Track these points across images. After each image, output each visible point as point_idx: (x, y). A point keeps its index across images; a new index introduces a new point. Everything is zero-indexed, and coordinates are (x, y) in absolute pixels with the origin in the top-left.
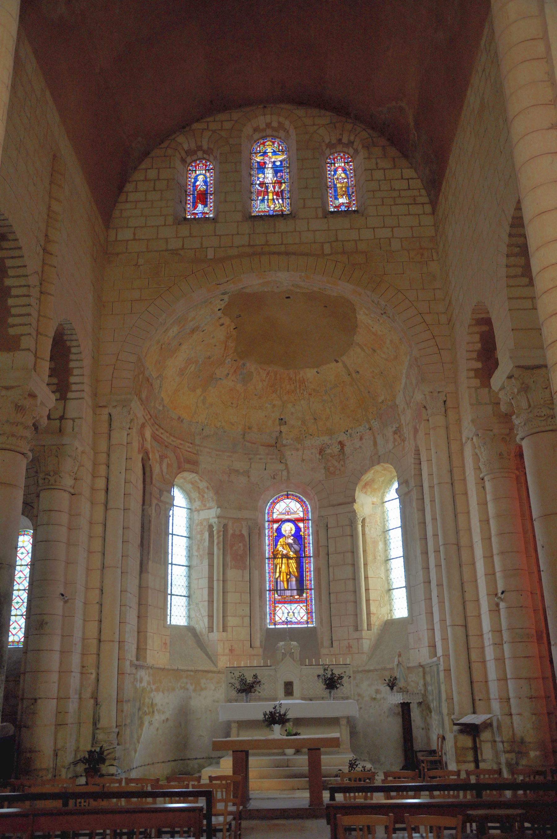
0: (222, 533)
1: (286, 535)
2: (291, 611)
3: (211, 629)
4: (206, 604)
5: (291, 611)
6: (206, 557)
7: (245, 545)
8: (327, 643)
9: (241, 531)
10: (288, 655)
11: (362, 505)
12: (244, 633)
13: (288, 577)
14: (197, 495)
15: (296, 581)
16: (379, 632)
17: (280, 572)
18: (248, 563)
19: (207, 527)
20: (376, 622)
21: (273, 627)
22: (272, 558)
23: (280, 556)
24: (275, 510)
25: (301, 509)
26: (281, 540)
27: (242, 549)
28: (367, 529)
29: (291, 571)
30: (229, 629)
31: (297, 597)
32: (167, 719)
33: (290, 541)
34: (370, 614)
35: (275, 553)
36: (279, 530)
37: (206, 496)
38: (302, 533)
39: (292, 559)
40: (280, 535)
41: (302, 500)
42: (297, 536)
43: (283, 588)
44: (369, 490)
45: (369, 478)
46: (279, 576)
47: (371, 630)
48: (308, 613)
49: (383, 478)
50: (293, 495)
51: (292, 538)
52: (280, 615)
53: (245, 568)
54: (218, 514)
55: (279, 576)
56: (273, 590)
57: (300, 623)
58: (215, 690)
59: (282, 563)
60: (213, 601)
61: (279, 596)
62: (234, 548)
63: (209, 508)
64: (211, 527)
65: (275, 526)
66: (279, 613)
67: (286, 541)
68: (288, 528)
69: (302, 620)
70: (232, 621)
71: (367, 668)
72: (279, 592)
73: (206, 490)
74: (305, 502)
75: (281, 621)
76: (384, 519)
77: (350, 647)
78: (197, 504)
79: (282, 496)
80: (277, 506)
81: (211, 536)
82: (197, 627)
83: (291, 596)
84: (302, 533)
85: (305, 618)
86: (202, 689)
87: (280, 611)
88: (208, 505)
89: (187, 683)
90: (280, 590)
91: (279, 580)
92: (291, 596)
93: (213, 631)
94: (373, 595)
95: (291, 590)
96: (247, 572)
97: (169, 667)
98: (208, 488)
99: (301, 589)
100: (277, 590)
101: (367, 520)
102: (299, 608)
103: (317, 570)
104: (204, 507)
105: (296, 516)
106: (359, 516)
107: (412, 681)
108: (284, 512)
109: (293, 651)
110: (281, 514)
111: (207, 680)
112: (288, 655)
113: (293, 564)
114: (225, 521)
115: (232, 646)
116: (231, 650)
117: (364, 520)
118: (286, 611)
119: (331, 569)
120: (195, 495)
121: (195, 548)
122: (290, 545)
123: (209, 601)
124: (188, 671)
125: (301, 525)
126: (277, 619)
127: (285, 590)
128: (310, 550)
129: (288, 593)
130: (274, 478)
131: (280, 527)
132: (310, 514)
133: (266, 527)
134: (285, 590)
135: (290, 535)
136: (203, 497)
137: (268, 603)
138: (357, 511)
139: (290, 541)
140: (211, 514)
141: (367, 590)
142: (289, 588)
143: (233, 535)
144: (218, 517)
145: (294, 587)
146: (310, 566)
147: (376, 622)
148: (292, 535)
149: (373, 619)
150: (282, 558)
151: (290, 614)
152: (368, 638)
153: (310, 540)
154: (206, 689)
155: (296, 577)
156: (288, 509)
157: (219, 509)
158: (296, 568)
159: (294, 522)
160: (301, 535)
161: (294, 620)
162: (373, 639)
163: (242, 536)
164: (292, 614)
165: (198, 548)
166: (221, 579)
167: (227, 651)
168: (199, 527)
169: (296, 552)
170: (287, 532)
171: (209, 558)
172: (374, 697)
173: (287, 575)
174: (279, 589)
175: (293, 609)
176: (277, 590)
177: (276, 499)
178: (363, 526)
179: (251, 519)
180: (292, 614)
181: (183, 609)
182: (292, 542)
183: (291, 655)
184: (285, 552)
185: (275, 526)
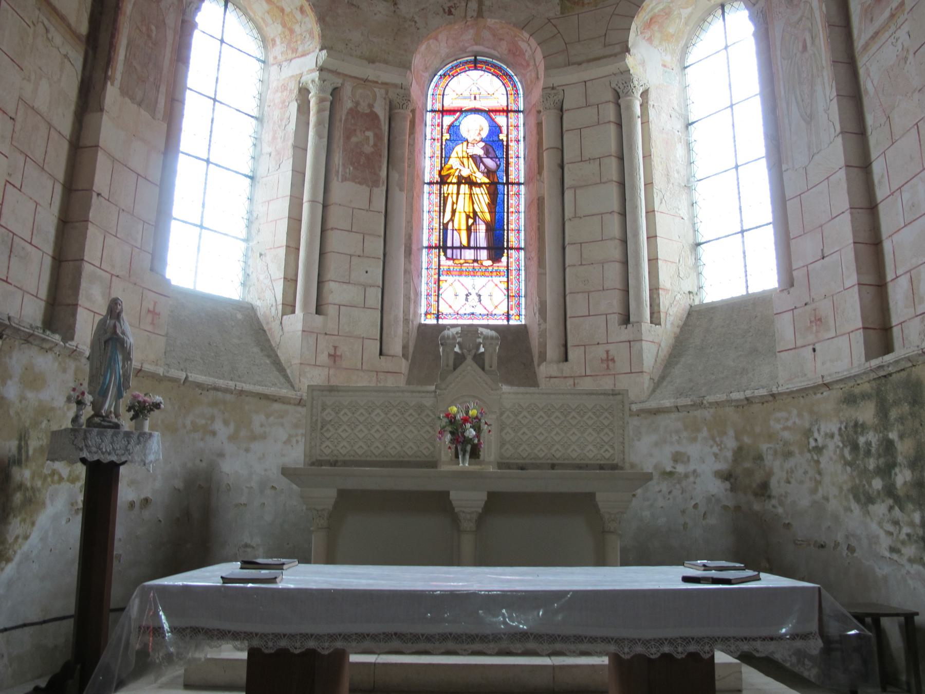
0: (328, 104)
1: (470, 140)
2: (473, 292)
3: (289, 307)
4: (282, 252)
6: (289, 152)
7: (378, 137)
8: (552, 352)
9: (371, 106)
10: (469, 360)
11: (643, 63)
12: (368, 322)
14: (280, 28)
15: (487, 230)
16: (678, 330)
17: (454, 212)
18: (384, 173)
19: (296, 91)
20: (673, 306)
21: (434, 322)
22: (437, 183)
27: (372, 142)
28: (652, 113)
29: (477, 209)
30: (331, 310)
32: (146, 501)
33: (478, 150)
34: (658, 289)
35: (444, 173)
37: (297, 28)
38: (503, 137)
39: (479, 185)
41: (507, 74)
42: (494, 144)
43: (458, 245)
44: (658, 35)
45: (661, 7)
46: (452, 220)
47: (660, 324)
49: (689, 10)
50: (486, 63)
51: (482, 144)
53: (375, 183)
54: (320, 63)
55: (452, 220)
56: (436, 247)
58: (287, 442)
59: (458, 194)
60: (298, 249)
61: (448, 259)
62: (354, 139)
63: (304, 55)
64: (303, 92)
65: (448, 120)
68: (474, 128)
70: (336, 292)
71: (653, 404)
72: (449, 252)
73: (298, 16)
74: (511, 77)
76: (686, 100)
77: (609, 359)
78: (278, 50)
79: (466, 63)
81: (303, 109)
82: (257, 303)
83: (476, 261)
84: (503, 137)
86: (254, 438)
88: (300, 49)
89: (213, 418)
90: (453, 248)
91: (450, 226)
92: (476, 261)
93: (293, 312)
94: (664, 249)
95: (477, 248)
96: (380, 192)
97: (161, 371)
98: (302, 10)
100: (445, 248)
101: (652, 96)
103: (537, 206)
104: (295, 52)
106: (636, 83)
107: (785, 428)
108: (466, 94)
109: (482, 350)
110: (461, 96)
111: (268, 416)
112: (469, 360)
113: (482, 197)
114: (338, 81)
115: (335, 348)
116: (334, 357)
117: (645, 94)
119: (568, 195)
120: (274, 30)
121: (267, 137)
122: (476, 159)
123: (287, 247)
124: (216, 389)
125: (501, 120)
127: (462, 247)
128: (518, 170)
129: (469, 254)
130: (450, 13)
131: (457, 123)
132: (521, 100)
134: (462, 247)
135: (478, 139)
136: (292, 31)
137: (424, 272)
138: (631, 72)
139: (478, 150)
140: (306, 65)
141: (652, 238)
142: (472, 244)
143: (354, 113)
144: (321, 69)
145: (483, 243)
146: (517, 204)
147: (673, 306)
148: (482, 140)
149: (664, 300)
150: (459, 184)
152: (655, 340)
153: (518, 151)
154: (263, 437)
155: (487, 224)
157: (324, 52)
158: (489, 205)
159: (488, 113)
160: (502, 141)
161: (479, 310)
162: (663, 345)
163: (373, 117)
164: (477, 298)
165: (274, 138)
166: (321, 199)
167: (323, 358)
168: (279, 94)
169: (489, 173)
171: (294, 156)
172: (668, 469)
173: (468, 217)
174: (449, 244)
176: (445, 248)
177: (452, 68)
178: (644, 106)
179: (395, 86)
180: (474, 297)
183: (479, 360)
184: (465, 173)
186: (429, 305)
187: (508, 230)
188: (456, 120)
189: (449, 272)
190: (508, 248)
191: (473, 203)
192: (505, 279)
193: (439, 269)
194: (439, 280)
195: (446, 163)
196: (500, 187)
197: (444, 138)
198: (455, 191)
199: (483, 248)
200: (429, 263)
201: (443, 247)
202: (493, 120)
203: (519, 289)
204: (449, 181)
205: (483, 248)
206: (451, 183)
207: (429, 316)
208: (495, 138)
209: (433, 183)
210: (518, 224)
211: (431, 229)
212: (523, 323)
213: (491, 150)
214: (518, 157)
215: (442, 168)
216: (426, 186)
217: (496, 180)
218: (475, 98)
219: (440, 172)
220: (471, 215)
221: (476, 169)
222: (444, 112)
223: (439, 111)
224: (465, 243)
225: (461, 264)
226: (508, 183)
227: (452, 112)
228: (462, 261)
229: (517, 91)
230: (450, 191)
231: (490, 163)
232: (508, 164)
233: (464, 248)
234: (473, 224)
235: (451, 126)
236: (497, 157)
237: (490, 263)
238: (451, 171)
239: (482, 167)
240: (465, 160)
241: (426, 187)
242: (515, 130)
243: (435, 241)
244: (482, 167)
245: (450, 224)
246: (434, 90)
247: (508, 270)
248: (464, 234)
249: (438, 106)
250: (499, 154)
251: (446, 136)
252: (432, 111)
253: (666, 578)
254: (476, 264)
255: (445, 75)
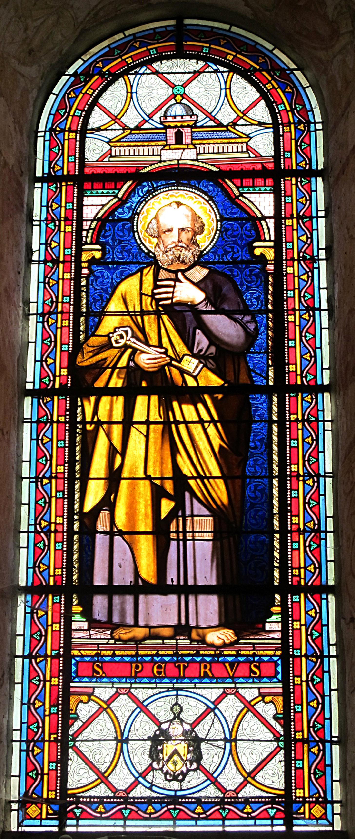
2: (176, 730)
5: (176, 730)
13: (166, 506)
15: (218, 535)
17: (114, 478)
22: (63, 391)
23: (117, 382)
24: (97, 118)
25: (262, 113)
26: (129, 286)
29: (187, 469)
31: (214, 637)
35: (85, 360)
36: (116, 227)
39: (194, 396)
40: (120, 251)
41: (273, 67)
42: (235, 268)
43: (128, 579)
46: (108, 502)
48: (288, 744)
50: (211, 36)
51: (199, 273)
52: (102, 755)
55: (108, 502)
56: (56, 590)
57: (229, 803)
59: (128, 423)
65: (95, 205)
66: (95, 740)
67: (163, 293)
68: (175, 218)
69: (249, 791)
72: (100, 602)
75: (102, 791)
79: (154, 36)
80: (114, 97)
83: (182, 629)
85: (273, 777)
87: (103, 727)
90: (110, 590)
91: (102, 524)
95: (186, 590)
99: (247, 590)
102: (231, 707)
105: (222, 153)
113: (204, 441)
118: (144, 727)
122: (185, 318)
126: (79, 776)
127: (139, 588)
128: (317, 348)
129: (161, 610)
132: (318, 139)
133: (38, 212)
134: (139, 588)
135: (188, 255)
139: (188, 292)
142: (172, 577)
145: (206, 574)
148: (200, 260)
150: (129, 394)
151: (168, 748)
155: (216, 512)
156: (178, 110)
158: (222, 456)
169: (221, 357)
170: (171, 239)
173: (158, 494)
174: (100, 579)
175: (189, 715)
181: (105, 97)
182: (197, 296)
184: (147, 359)
185: (95, 205)
186: (32, 772)
187: (284, 531)
188: (122, 202)
189: (99, 667)
190: (287, 589)
191: (174, 452)
192: (277, 687)
193: (68, 657)
194: (67, 693)
195: (91, 331)
196: (258, 401)
197: (85, 257)
198: (118, 415)
199: (207, 590)
200: (37, 636)
201: (78, 588)
202: (234, 200)
203: (323, 719)
204: (100, 384)
205: (207, 590)
206: (108, 391)
207: (33, 810)
208: (242, 255)
209: (52, 392)
210: (316, 509)
211: (41, 532)
212: (338, 827)
213: (227, 289)
214: (311, 309)
215: (78, 347)
216: (28, 400)
217: (244, 378)
218: (179, 139)
219: (72, 357)
220: (169, 486)
221: (181, 348)
222: (86, 179)
223: (69, 178)
224: (148, 571)
225: (137, 641)
226: (282, 388)
227: (106, 179)
228: (140, 632)
229: (305, 112)
230: (103, 415)
231: (225, 327)
232: (280, 330)
233: (148, 589)
234: (173, 514)
235: (105, 221)
236: (246, 311)
237: (227, 635)
238: (110, 354)
239: (202, 341)
240: (150, 324)
241: (29, 407)
242: (306, 231)
243: (54, 572)
244: (202, 341)
245: (104, 515)
246: (56, 116)
247: (285, 657)
248: (146, 547)
249: (66, 164)
250: (251, 298)
251: (92, 252)
252: (49, 179)
253: (76, 190)
254: (183, 641)
255: (87, 74)
